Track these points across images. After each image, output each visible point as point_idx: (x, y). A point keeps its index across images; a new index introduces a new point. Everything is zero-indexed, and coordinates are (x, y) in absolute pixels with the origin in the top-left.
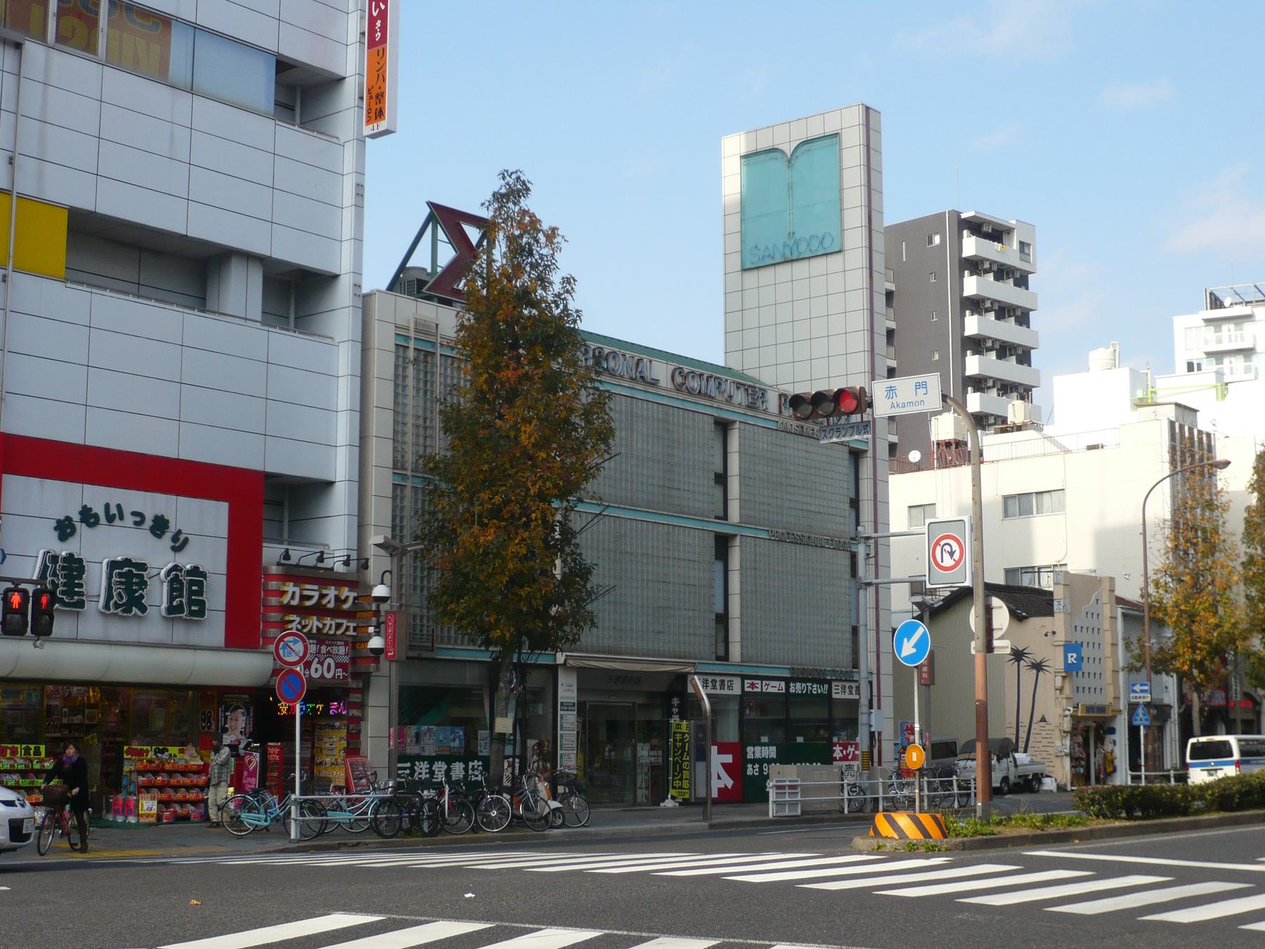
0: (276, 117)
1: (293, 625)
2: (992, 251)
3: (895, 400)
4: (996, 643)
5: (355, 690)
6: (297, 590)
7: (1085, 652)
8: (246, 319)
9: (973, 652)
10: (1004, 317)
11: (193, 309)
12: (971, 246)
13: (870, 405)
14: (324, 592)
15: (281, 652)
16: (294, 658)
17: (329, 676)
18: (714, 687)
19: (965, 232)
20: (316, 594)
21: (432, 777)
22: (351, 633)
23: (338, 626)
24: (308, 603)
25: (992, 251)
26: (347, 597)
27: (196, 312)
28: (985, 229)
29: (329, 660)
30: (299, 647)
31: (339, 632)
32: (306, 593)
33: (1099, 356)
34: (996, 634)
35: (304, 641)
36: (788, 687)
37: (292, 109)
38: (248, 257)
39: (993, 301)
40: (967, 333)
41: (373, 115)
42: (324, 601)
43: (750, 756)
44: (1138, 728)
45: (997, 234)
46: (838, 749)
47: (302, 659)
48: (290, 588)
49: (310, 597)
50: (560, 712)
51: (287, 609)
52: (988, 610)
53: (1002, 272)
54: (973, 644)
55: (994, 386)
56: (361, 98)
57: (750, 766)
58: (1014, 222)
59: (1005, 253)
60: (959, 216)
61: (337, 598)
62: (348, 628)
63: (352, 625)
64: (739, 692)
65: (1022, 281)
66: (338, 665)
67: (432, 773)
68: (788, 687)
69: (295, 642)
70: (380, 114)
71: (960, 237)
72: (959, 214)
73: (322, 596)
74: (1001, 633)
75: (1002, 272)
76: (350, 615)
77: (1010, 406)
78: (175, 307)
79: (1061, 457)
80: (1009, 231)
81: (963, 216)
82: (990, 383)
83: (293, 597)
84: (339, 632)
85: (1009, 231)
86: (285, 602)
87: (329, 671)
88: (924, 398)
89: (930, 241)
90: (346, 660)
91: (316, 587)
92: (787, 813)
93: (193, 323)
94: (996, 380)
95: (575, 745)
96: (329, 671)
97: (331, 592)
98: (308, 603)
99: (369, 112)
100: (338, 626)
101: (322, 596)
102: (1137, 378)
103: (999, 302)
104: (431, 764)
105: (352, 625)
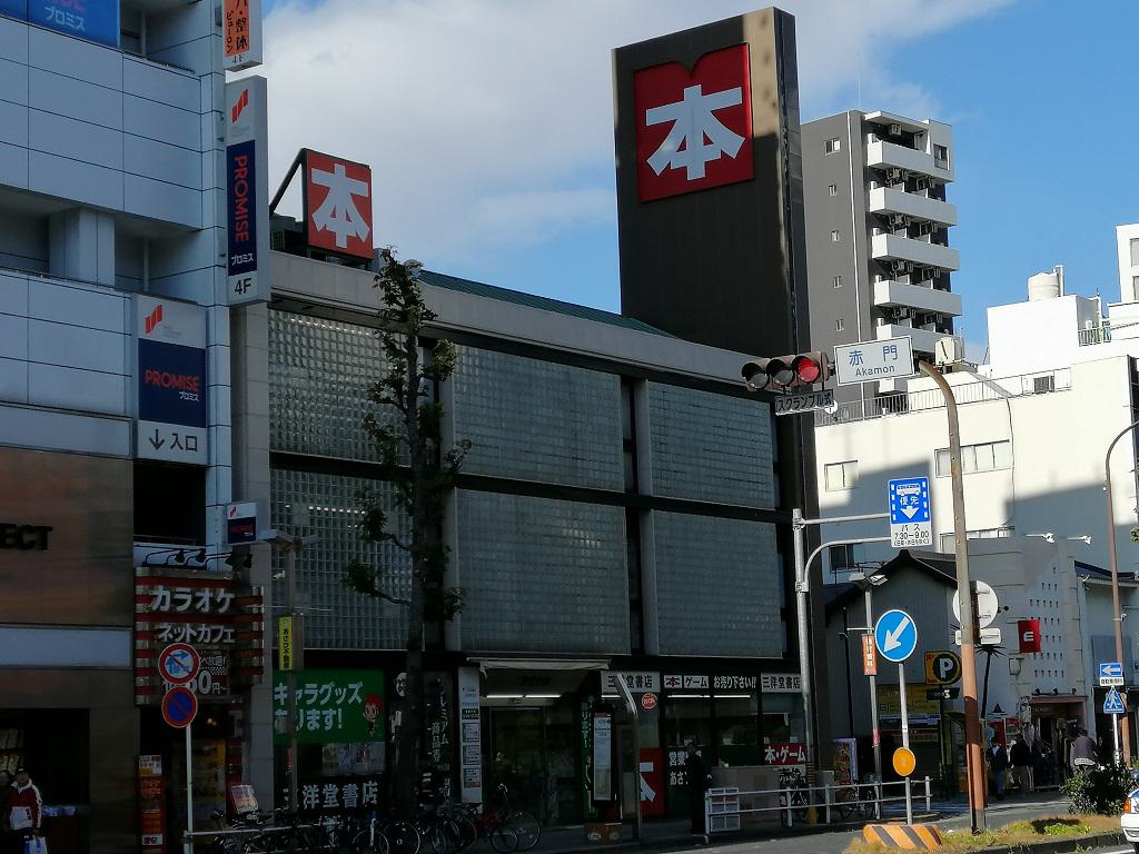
0: (126, 50)
1: (164, 635)
2: (903, 158)
3: (860, 366)
4: (983, 632)
5: (237, 706)
6: (168, 593)
7: (1043, 630)
8: (98, 285)
9: (958, 643)
10: (918, 235)
11: (39, 275)
12: (876, 152)
13: (833, 372)
14: (198, 594)
15: (167, 668)
16: (182, 674)
17: (206, 691)
18: (639, 685)
19: (870, 135)
20: (189, 598)
21: (322, 803)
22: (229, 640)
23: (215, 633)
24: (181, 608)
25: (903, 158)
26: (224, 600)
27: (42, 279)
28: (893, 132)
29: (205, 673)
30: (188, 661)
31: (215, 641)
32: (177, 596)
33: (1040, 283)
34: (983, 623)
35: (193, 654)
36: (712, 682)
37: (137, 37)
38: (98, 212)
39: (905, 217)
40: (875, 255)
41: (234, 44)
42: (199, 605)
43: (673, 763)
44: (1110, 716)
45: (908, 138)
46: (770, 751)
47: (191, 674)
48: (160, 592)
49: (183, 602)
50: (462, 721)
51: (156, 616)
52: (974, 595)
53: (914, 182)
54: (958, 633)
55: (908, 317)
56: (219, 24)
57: (673, 774)
58: (927, 122)
59: (918, 160)
60: (862, 118)
61: (212, 600)
62: (225, 634)
63: (229, 631)
64: (658, 691)
65: (938, 191)
66: (214, 679)
67: (322, 797)
68: (712, 682)
69: (184, 655)
70: (243, 43)
71: (864, 142)
72: (862, 116)
73: (196, 600)
74: (990, 620)
75: (914, 182)
76: (226, 620)
77: (938, 344)
78: (17, 274)
79: (1004, 403)
80: (922, 133)
81: (868, 117)
82: (904, 313)
83: (163, 603)
84: (215, 641)
85: (922, 133)
86: (154, 608)
87: (205, 685)
88: (893, 363)
89: (829, 148)
90: (223, 672)
91: (188, 590)
92: (726, 829)
93: (42, 292)
94: (910, 309)
95: (479, 757)
96: (205, 685)
97: (206, 594)
98: (181, 608)
99: (229, 40)
100: (215, 633)
101: (196, 600)
102: (1085, 308)
103: (911, 217)
104: (321, 788)
105: (229, 631)
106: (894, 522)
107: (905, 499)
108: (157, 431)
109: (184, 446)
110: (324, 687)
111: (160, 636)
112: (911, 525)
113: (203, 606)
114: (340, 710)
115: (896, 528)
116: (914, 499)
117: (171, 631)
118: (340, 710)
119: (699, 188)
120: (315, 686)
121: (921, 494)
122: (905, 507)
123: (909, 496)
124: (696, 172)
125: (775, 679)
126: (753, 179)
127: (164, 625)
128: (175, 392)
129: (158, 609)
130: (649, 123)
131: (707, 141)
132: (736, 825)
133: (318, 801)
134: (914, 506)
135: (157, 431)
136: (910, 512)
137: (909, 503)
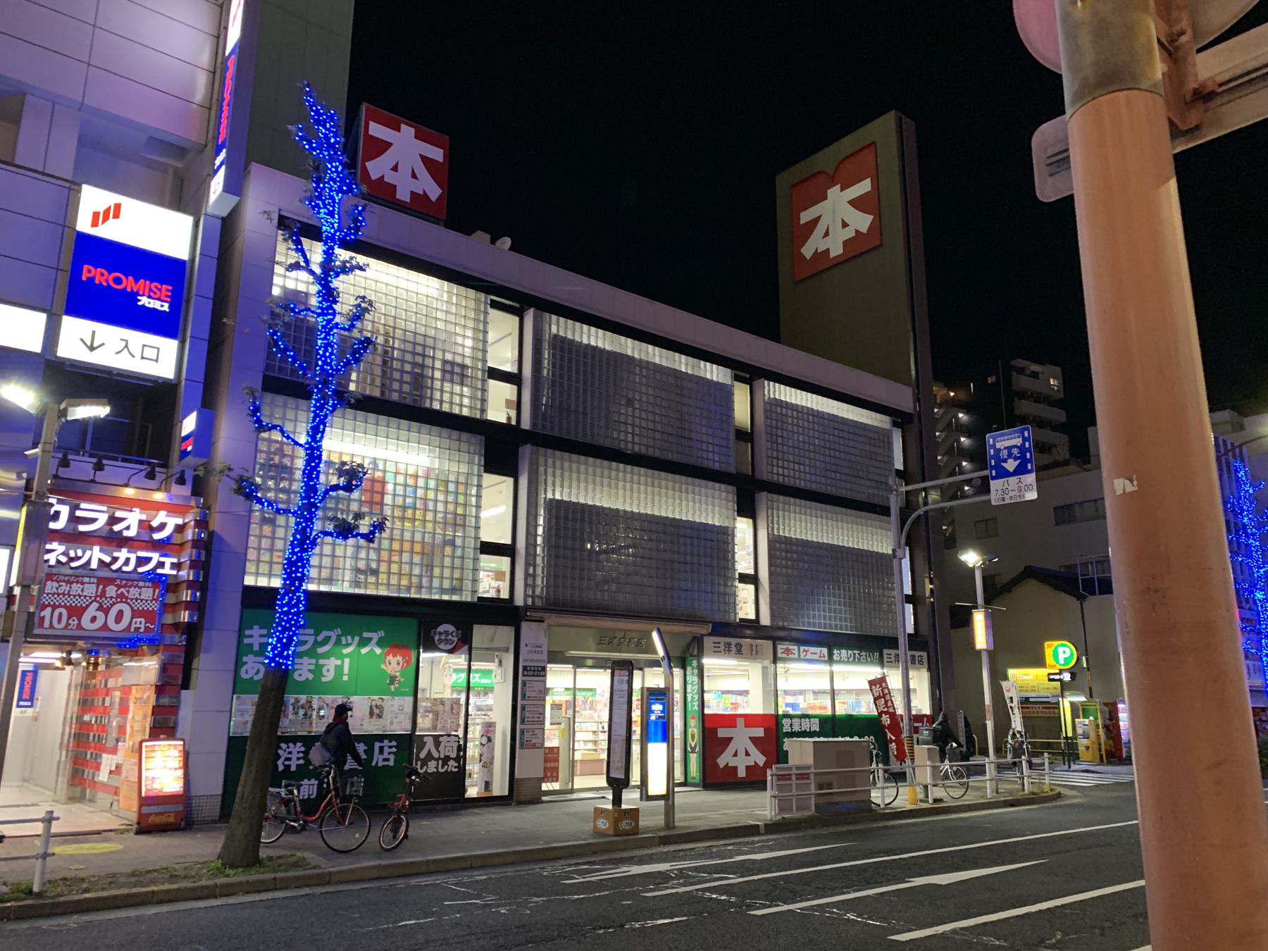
32: (78, 513)
66: (136, 614)
87: (59, 621)
91: (104, 508)
106: (993, 478)
107: (1005, 452)
108: (94, 333)
109: (138, 355)
110: (325, 634)
111: (46, 557)
112: (1013, 480)
113: (128, 528)
114: (347, 661)
115: (995, 485)
116: (1015, 451)
117: (65, 554)
118: (347, 661)
119: (842, 262)
120: (312, 631)
121: (1023, 444)
122: (1005, 461)
123: (1009, 448)
124: (837, 251)
125: (729, 644)
126: (881, 245)
127: (54, 545)
128: (134, 296)
129: (121, 532)
130: (802, 222)
131: (845, 225)
132: (808, 808)
133: (302, 762)
134: (1015, 459)
135: (94, 333)
136: (1011, 465)
137: (1010, 455)
